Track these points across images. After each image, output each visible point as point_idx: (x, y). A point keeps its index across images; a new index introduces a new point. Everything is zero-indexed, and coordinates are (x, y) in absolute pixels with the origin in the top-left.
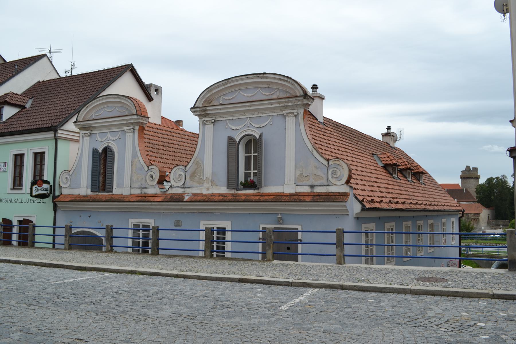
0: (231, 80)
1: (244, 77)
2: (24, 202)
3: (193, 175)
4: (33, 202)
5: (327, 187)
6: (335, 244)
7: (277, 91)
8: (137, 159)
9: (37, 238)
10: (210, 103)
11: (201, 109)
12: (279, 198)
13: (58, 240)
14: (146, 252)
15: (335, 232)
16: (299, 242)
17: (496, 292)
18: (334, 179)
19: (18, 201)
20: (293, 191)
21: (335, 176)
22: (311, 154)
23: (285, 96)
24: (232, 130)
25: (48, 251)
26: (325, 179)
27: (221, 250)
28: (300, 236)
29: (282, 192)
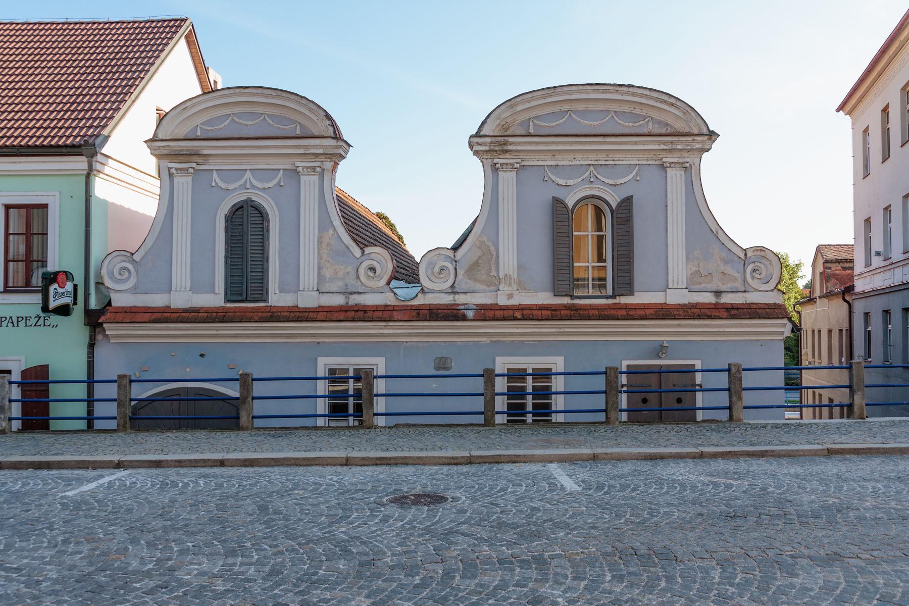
0: (558, 90)
1: (588, 87)
3: (474, 268)
4: (10, 324)
5: (744, 294)
7: (649, 120)
8: (331, 232)
9: (55, 410)
10: (506, 130)
11: (494, 139)
12: (663, 313)
13: (100, 409)
15: (115, 381)
16: (698, 388)
17: (410, 469)
18: (756, 281)
20: (684, 301)
21: (758, 276)
22: (715, 237)
23: (663, 131)
24: (557, 186)
25: (75, 438)
26: (740, 280)
27: (543, 411)
28: (699, 377)
29: (662, 301)
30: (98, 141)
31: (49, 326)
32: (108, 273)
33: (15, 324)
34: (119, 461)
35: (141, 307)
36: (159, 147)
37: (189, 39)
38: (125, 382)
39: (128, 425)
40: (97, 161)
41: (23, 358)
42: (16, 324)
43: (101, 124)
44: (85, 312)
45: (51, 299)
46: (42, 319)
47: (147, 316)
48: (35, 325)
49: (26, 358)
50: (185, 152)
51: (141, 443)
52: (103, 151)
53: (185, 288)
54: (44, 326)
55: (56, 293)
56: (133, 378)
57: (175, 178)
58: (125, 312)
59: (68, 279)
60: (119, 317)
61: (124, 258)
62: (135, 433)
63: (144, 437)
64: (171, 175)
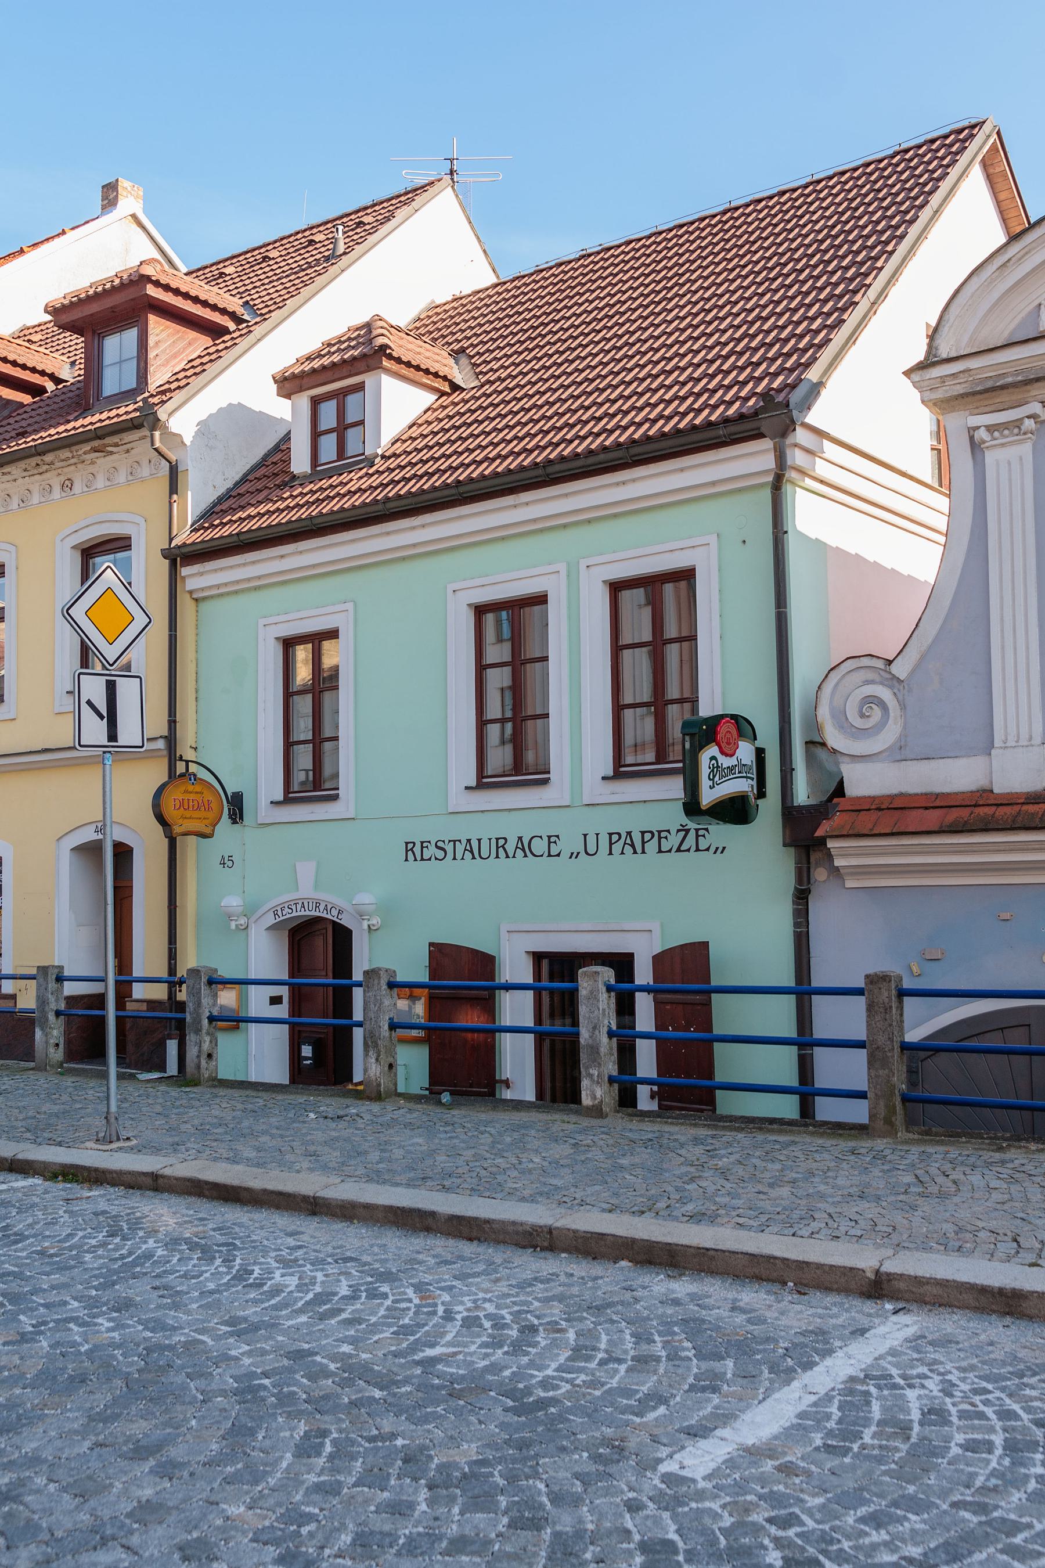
2: (565, 855)
4: (628, 849)
6: (859, 1045)
14: (554, 1100)
15: (859, 992)
19: (525, 847)
30: (795, 397)
31: (708, 849)
32: (833, 716)
33: (639, 848)
34: (877, 1272)
35: (916, 795)
36: (943, 379)
37: (991, 171)
38: (888, 994)
39: (899, 1119)
40: (796, 445)
41: (655, 926)
42: (639, 849)
43: (802, 361)
44: (784, 814)
45: (705, 782)
46: (692, 833)
47: (933, 818)
48: (679, 850)
49: (662, 925)
50: (1010, 380)
51: (942, 1196)
52: (811, 418)
53: (1030, 739)
54: (697, 850)
55: (716, 769)
56: (907, 984)
57: (987, 453)
58: (879, 809)
59: (741, 735)
60: (865, 822)
61: (870, 675)
62: (919, 1142)
63: (947, 1167)
64: (976, 447)
